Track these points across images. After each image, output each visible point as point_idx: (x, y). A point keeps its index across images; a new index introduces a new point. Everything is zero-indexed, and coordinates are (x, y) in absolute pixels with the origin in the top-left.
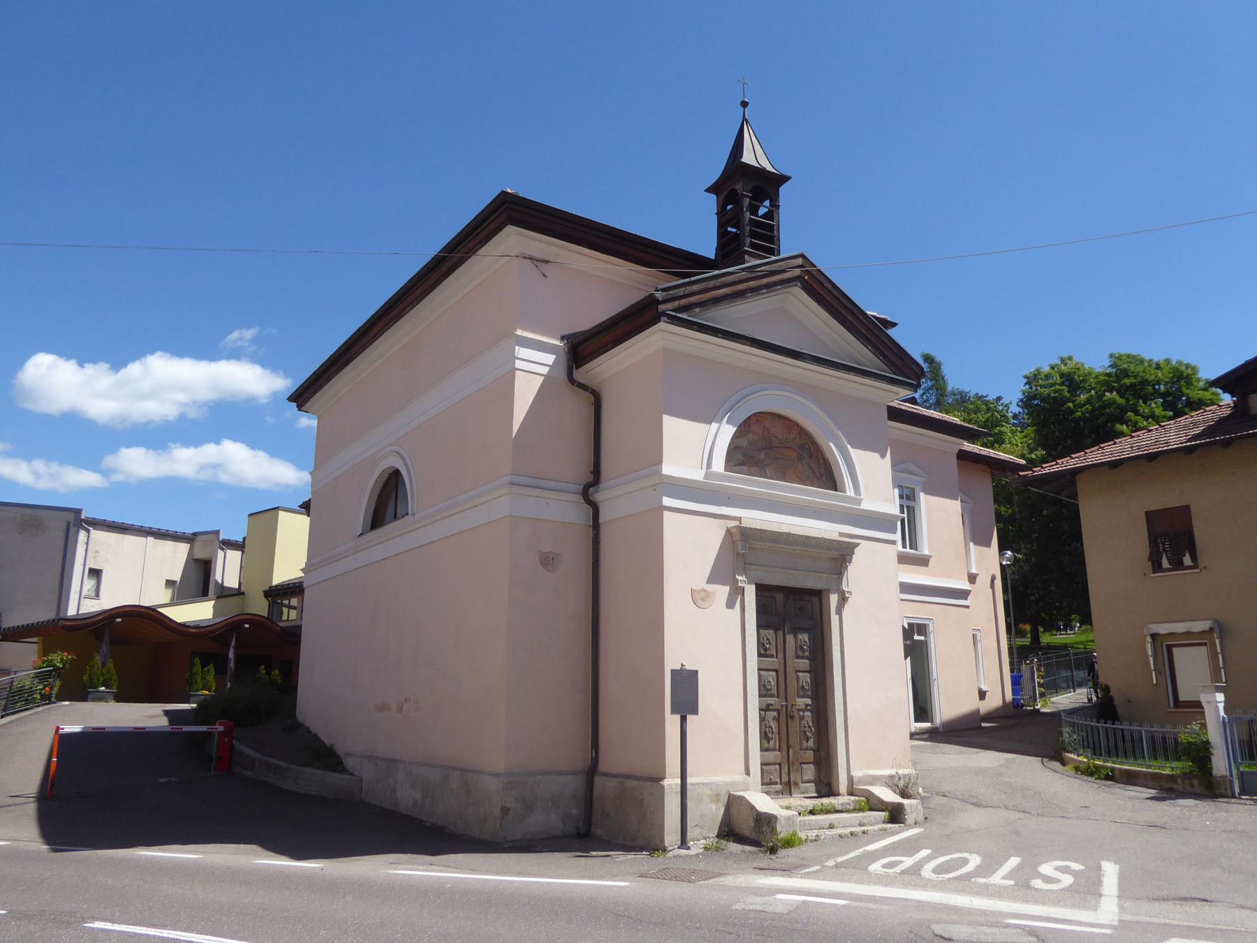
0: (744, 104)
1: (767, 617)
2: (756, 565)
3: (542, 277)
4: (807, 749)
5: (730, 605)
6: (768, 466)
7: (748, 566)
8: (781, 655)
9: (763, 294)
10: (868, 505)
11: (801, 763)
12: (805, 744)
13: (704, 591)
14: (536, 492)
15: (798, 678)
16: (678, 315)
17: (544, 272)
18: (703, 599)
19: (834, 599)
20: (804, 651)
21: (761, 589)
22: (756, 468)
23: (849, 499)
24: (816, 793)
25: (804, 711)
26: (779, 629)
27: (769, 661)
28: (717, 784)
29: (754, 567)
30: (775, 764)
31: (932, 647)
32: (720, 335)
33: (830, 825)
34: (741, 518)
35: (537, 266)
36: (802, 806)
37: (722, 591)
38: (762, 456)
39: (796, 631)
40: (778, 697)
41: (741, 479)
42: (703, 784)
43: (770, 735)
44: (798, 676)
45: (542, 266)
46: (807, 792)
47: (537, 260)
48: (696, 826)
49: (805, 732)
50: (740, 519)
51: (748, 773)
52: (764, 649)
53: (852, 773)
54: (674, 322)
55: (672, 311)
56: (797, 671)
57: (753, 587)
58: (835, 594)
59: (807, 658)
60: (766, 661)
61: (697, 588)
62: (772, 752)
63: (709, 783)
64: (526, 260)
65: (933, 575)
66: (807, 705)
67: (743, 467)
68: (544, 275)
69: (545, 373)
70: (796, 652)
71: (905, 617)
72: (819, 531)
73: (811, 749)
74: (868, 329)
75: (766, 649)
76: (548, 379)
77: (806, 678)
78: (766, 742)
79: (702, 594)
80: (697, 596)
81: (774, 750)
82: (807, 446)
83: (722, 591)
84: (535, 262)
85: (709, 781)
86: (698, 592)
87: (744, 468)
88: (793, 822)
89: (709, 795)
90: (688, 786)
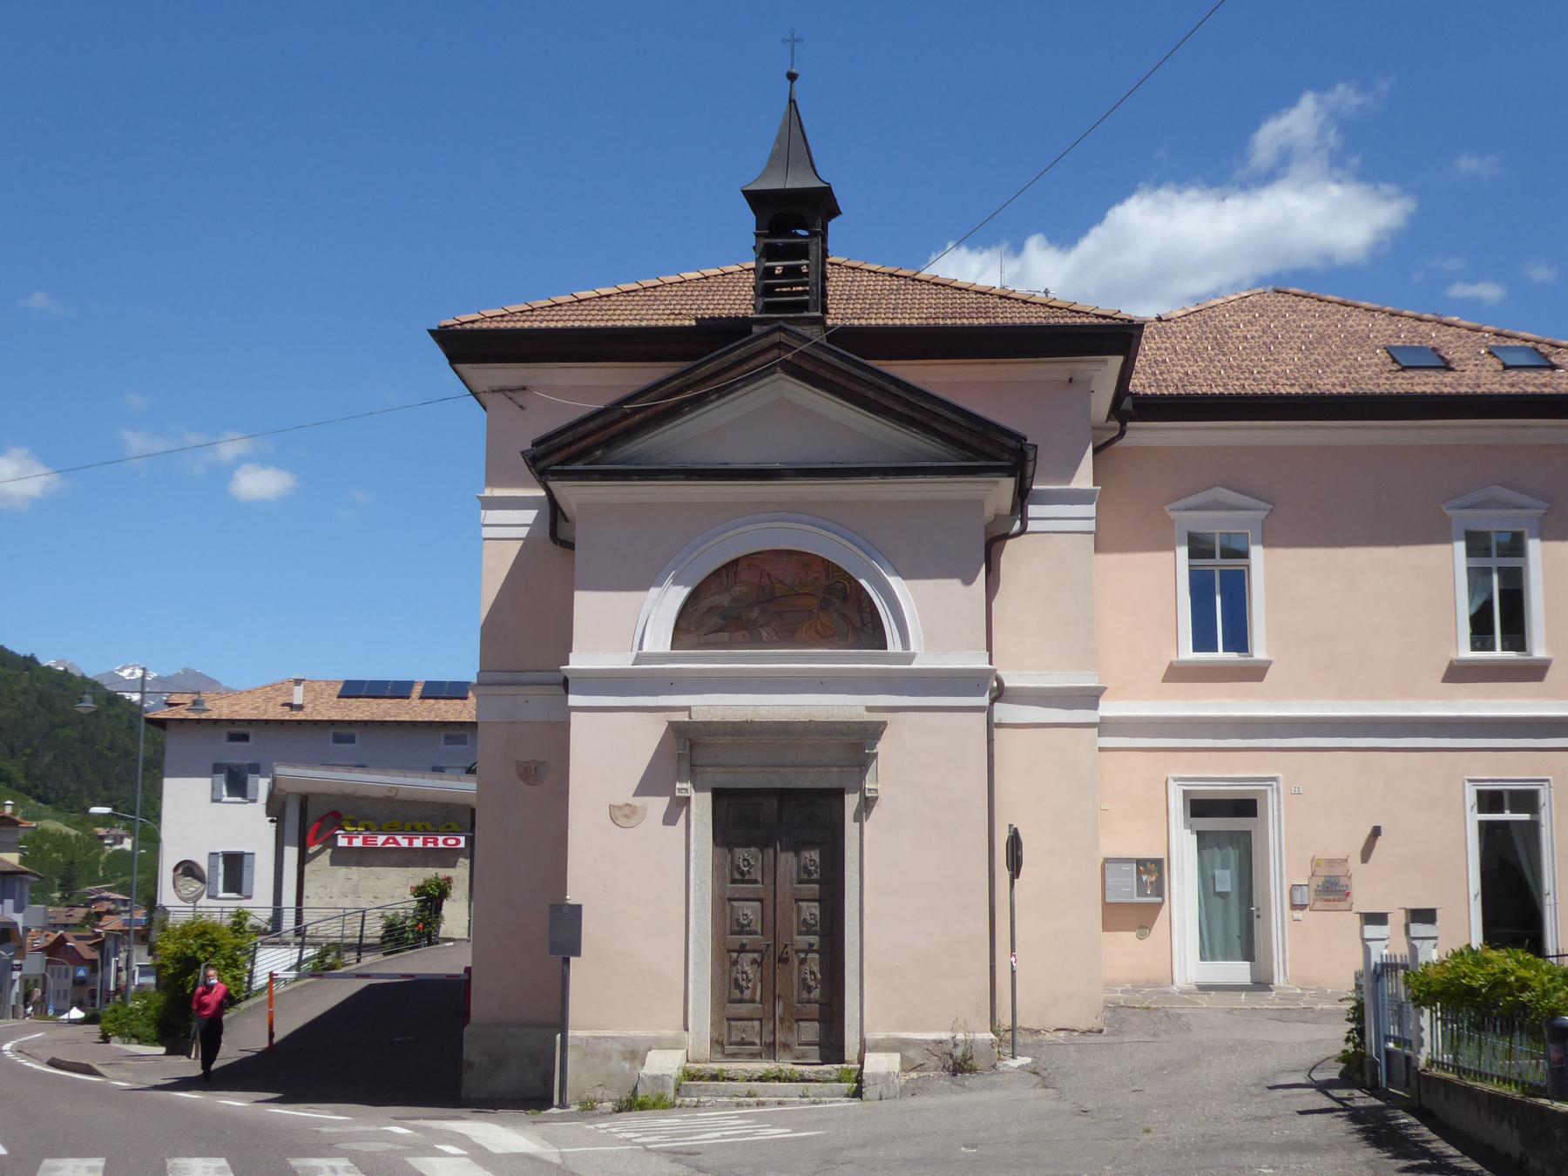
0: (792, 77)
1: (727, 832)
2: (710, 766)
3: (519, 408)
4: (809, 1002)
5: (670, 819)
6: (762, 626)
7: (698, 769)
8: (769, 880)
9: (712, 401)
10: (926, 660)
11: (797, 1020)
12: (805, 995)
13: (629, 805)
14: (509, 690)
15: (799, 909)
16: (566, 468)
17: (520, 404)
18: (627, 816)
19: (851, 802)
20: (810, 873)
21: (719, 795)
22: (745, 632)
23: (896, 658)
24: (820, 1059)
25: (807, 952)
26: (767, 846)
27: (749, 888)
28: (633, 1039)
29: (709, 769)
30: (752, 1019)
31: (1545, 832)
32: (636, 478)
33: (749, 1092)
34: (690, 707)
35: (511, 399)
36: (746, 1071)
37: (658, 805)
38: (755, 613)
39: (796, 847)
40: (762, 935)
41: (694, 655)
42: (612, 1038)
43: (744, 984)
44: (732, 907)
45: (517, 396)
46: (804, 1057)
47: (509, 390)
48: (600, 1085)
49: (805, 979)
50: (688, 709)
51: (686, 1029)
52: (739, 873)
53: (867, 1036)
54: (562, 478)
55: (557, 465)
56: (797, 900)
57: (707, 797)
58: (854, 793)
59: (816, 882)
60: (742, 888)
61: (619, 802)
62: (748, 1005)
63: (623, 1037)
64: (495, 394)
65: (1554, 695)
66: (811, 945)
67: (721, 633)
68: (521, 407)
69: (524, 536)
70: (732, 874)
71: (1470, 781)
72: (830, 708)
73: (816, 1002)
74: (908, 404)
75: (742, 873)
76: (528, 544)
77: (812, 910)
78: (737, 992)
79: (627, 810)
80: (618, 813)
81: (752, 1001)
82: (839, 586)
83: (658, 805)
84: (507, 393)
85: (623, 1035)
86: (620, 808)
87: (724, 636)
88: (663, 1083)
89: (620, 1051)
90: (569, 1039)
